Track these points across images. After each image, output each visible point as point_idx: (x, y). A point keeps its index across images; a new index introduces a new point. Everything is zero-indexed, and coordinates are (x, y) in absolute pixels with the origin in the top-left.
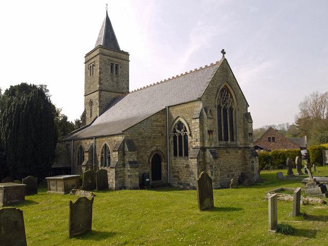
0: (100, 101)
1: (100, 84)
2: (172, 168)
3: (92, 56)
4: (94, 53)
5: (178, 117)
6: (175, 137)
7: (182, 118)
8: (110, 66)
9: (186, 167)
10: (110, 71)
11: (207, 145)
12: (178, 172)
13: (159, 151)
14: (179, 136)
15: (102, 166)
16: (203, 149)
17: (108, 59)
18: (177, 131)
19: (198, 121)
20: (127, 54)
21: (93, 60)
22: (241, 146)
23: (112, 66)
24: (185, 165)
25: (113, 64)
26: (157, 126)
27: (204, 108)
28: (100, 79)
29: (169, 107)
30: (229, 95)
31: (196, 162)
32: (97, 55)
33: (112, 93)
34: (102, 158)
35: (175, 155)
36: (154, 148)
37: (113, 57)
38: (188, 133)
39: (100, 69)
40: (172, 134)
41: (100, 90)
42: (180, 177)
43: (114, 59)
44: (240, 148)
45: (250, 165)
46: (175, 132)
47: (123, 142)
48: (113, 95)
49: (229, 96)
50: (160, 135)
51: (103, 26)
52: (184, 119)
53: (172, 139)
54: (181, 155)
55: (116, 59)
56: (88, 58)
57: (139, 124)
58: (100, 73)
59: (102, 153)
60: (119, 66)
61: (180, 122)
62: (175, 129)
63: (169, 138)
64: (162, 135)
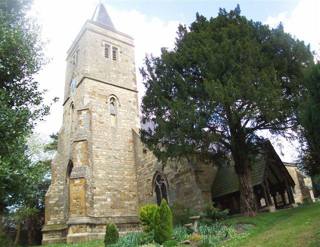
25: (109, 46)
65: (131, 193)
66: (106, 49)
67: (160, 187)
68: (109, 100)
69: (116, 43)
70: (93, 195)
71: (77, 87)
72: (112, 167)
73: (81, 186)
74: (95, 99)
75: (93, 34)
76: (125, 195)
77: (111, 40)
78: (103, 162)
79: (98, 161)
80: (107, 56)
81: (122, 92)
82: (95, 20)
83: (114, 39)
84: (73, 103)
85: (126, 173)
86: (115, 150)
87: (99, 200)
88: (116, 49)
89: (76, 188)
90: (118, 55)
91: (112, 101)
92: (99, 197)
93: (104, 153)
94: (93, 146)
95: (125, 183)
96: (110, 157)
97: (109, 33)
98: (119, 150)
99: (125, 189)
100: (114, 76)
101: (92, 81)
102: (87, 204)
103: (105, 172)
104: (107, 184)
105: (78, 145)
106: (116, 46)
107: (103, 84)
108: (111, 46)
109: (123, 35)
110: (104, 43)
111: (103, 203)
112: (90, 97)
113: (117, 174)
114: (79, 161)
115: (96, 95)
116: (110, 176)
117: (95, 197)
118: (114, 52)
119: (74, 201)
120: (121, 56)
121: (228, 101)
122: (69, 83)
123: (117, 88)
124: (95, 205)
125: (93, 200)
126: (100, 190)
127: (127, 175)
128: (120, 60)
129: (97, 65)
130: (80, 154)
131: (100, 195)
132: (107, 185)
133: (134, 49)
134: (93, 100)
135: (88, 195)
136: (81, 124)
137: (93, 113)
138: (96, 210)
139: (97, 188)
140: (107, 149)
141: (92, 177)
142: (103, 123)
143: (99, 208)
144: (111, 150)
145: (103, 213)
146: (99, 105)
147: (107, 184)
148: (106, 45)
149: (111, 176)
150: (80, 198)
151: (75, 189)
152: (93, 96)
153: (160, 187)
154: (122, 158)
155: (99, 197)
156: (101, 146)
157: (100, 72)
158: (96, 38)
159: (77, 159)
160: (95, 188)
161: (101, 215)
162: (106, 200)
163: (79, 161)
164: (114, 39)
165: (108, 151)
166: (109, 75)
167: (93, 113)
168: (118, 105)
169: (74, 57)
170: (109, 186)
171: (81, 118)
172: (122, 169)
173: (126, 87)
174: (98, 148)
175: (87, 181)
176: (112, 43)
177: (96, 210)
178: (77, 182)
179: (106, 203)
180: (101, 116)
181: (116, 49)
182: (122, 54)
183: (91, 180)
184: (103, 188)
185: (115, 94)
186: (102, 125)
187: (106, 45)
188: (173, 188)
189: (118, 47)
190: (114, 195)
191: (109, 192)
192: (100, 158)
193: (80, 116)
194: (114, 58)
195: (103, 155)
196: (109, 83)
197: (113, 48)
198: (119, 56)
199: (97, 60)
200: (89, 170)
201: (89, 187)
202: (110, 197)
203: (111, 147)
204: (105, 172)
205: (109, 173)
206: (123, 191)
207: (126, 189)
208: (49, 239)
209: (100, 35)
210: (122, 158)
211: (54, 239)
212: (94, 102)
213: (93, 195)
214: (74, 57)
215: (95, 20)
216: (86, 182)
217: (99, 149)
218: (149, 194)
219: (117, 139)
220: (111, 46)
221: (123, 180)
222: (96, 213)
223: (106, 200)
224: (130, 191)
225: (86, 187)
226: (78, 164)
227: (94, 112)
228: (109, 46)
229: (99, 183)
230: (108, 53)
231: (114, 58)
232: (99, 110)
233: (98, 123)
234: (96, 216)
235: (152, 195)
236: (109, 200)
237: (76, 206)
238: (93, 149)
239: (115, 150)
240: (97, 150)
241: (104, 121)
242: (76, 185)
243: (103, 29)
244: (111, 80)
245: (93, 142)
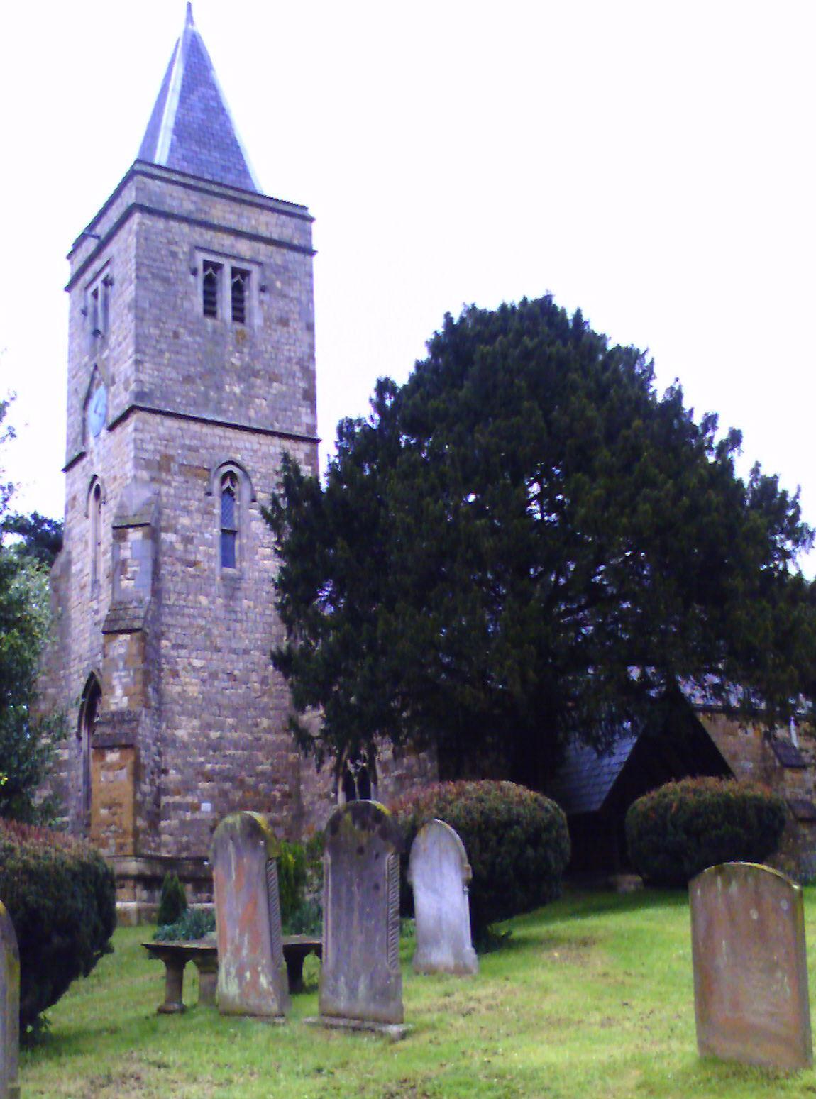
20: (299, 215)
21: (98, 264)
25: (218, 267)
60: (255, 279)
65: (278, 786)
66: (210, 285)
67: (355, 780)
68: (217, 483)
69: (244, 247)
70: (161, 791)
71: (111, 428)
72: (219, 706)
73: (124, 771)
74: (168, 484)
75: (161, 224)
76: (257, 793)
77: (227, 241)
78: (194, 690)
79: (178, 689)
80: (210, 309)
81: (264, 448)
82: (161, 157)
83: (238, 234)
84: (98, 482)
85: (265, 722)
86: (234, 651)
87: (178, 807)
88: (245, 274)
89: (111, 775)
90: (253, 298)
91: (228, 483)
92: (177, 799)
93: (197, 663)
94: (164, 643)
95: (260, 756)
96: (214, 676)
97: (221, 212)
98: (246, 652)
99: (257, 775)
100: (237, 390)
101: (158, 418)
102: (141, 823)
103: (196, 723)
104: (202, 759)
105: (116, 644)
106: (244, 266)
107: (196, 427)
108: (228, 265)
109: (273, 210)
110: (201, 257)
111: (189, 816)
112: (153, 479)
113: (234, 728)
114: (119, 692)
115: (174, 467)
116: (214, 735)
117: (165, 800)
118: (238, 289)
119: (104, 812)
120: (261, 302)
121: (103, 852)
122: (82, 395)
123: (246, 436)
124: (163, 823)
125: (158, 806)
126: (179, 777)
127: (268, 731)
128: (256, 318)
129: (177, 353)
130: (123, 674)
131: (178, 793)
132: (202, 763)
133: (315, 259)
134: (164, 489)
135: (144, 795)
136: (124, 572)
137: (163, 535)
138: (165, 838)
139: (172, 772)
140: (205, 649)
141: (159, 739)
142: (194, 564)
143: (176, 832)
144: (219, 650)
145: (187, 847)
146: (183, 503)
147: (202, 759)
148: (207, 264)
149: (218, 734)
150: (120, 805)
151: (106, 777)
152: (164, 475)
153: (355, 780)
154: (254, 677)
155: (177, 799)
156: (187, 641)
157: (188, 379)
158: (170, 243)
159: (112, 688)
160: (165, 772)
161: (179, 851)
162: (196, 808)
163: (119, 692)
164: (238, 234)
165: (208, 654)
166: (219, 388)
167: (163, 535)
168: (246, 495)
169: (95, 294)
170: (209, 766)
171: (126, 553)
172: (251, 712)
173: (277, 427)
174: (177, 646)
175: (143, 753)
176: (227, 256)
177: (165, 838)
178: (112, 757)
179: (198, 815)
180: (187, 540)
181: (245, 274)
182: (265, 297)
183: (154, 749)
184: (190, 772)
185: (238, 457)
186: (191, 570)
187: (207, 264)
188: (386, 787)
189: (254, 269)
190: (224, 794)
191: (207, 785)
192: (185, 678)
193: (123, 544)
194: (239, 314)
195: (194, 669)
196: (220, 419)
197: (235, 272)
198: (255, 303)
199: (176, 335)
200: (148, 721)
201: (148, 770)
202: (211, 798)
203: (219, 643)
204: (196, 723)
205: (209, 726)
206: (251, 781)
207: (263, 773)
208: (720, 900)
209: (185, 228)
210: (254, 677)
211: (330, 870)
212: (168, 495)
213: (161, 791)
214: (95, 294)
215: (161, 156)
216: (138, 757)
217: (183, 652)
218: (327, 796)
219: (239, 616)
220: (228, 265)
221: (256, 744)
222: (166, 845)
223: (196, 808)
224: (276, 781)
225: (137, 773)
226: (117, 699)
227: (166, 530)
228: (218, 267)
229: (178, 756)
230: (214, 294)
231: (239, 314)
232: (185, 521)
233: (179, 567)
234: (164, 854)
235: (335, 801)
236: (206, 807)
237: (109, 826)
238: (163, 651)
239: (234, 651)
240: (174, 653)
241: (199, 557)
242: (110, 767)
243: (195, 196)
244: (224, 405)
245: (164, 629)
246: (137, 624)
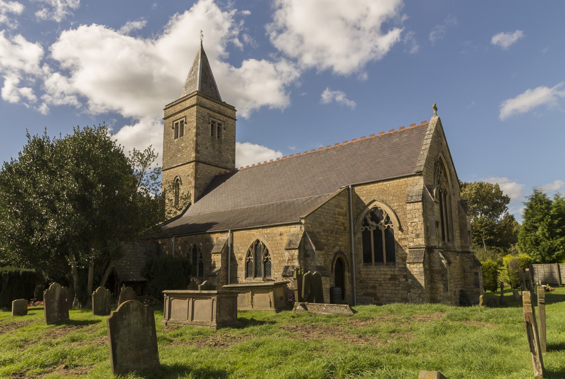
0: (196, 179)
1: (197, 151)
2: (361, 282)
3: (178, 108)
4: (183, 103)
5: (374, 201)
6: (366, 234)
7: (383, 201)
8: (210, 126)
9: (390, 279)
10: (210, 133)
11: (435, 243)
12: (374, 287)
13: (343, 253)
14: (199, 264)
15: (247, 276)
16: (429, 249)
17: (208, 113)
18: (370, 222)
19: (419, 205)
21: (182, 114)
22: (459, 250)
23: (212, 126)
24: (389, 276)
25: (214, 122)
26: (339, 214)
27: (427, 186)
28: (197, 145)
29: (353, 186)
30: (442, 171)
31: (422, 270)
32: (192, 106)
33: (213, 167)
34: (248, 264)
35: (367, 259)
36: (337, 249)
37: (215, 111)
38: (395, 226)
39: (197, 128)
40: (361, 229)
41: (197, 161)
42: (379, 295)
43: (216, 114)
44: (458, 252)
45: (471, 279)
46: (366, 223)
47: (304, 236)
48: (215, 171)
49: (442, 174)
50: (343, 228)
51: (195, 63)
52: (386, 204)
53: (360, 235)
54: (379, 259)
55: (218, 115)
56: (172, 111)
57: (320, 209)
58: (197, 135)
59: (249, 255)
60: (223, 126)
61: (376, 208)
62: (365, 220)
63: (355, 234)
64: (345, 229)
118: (218, 127)
246: (407, 204)
